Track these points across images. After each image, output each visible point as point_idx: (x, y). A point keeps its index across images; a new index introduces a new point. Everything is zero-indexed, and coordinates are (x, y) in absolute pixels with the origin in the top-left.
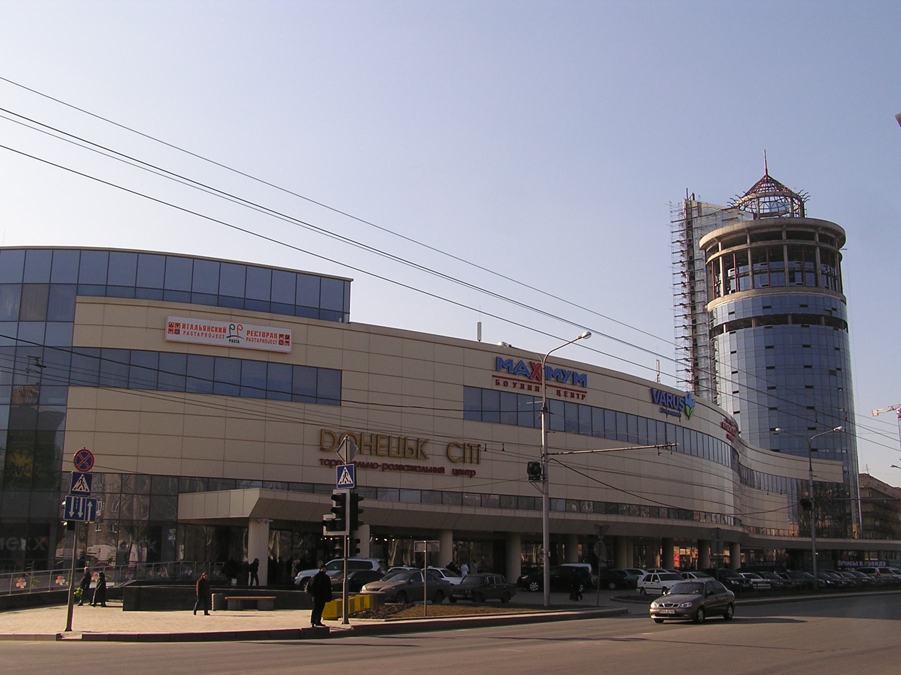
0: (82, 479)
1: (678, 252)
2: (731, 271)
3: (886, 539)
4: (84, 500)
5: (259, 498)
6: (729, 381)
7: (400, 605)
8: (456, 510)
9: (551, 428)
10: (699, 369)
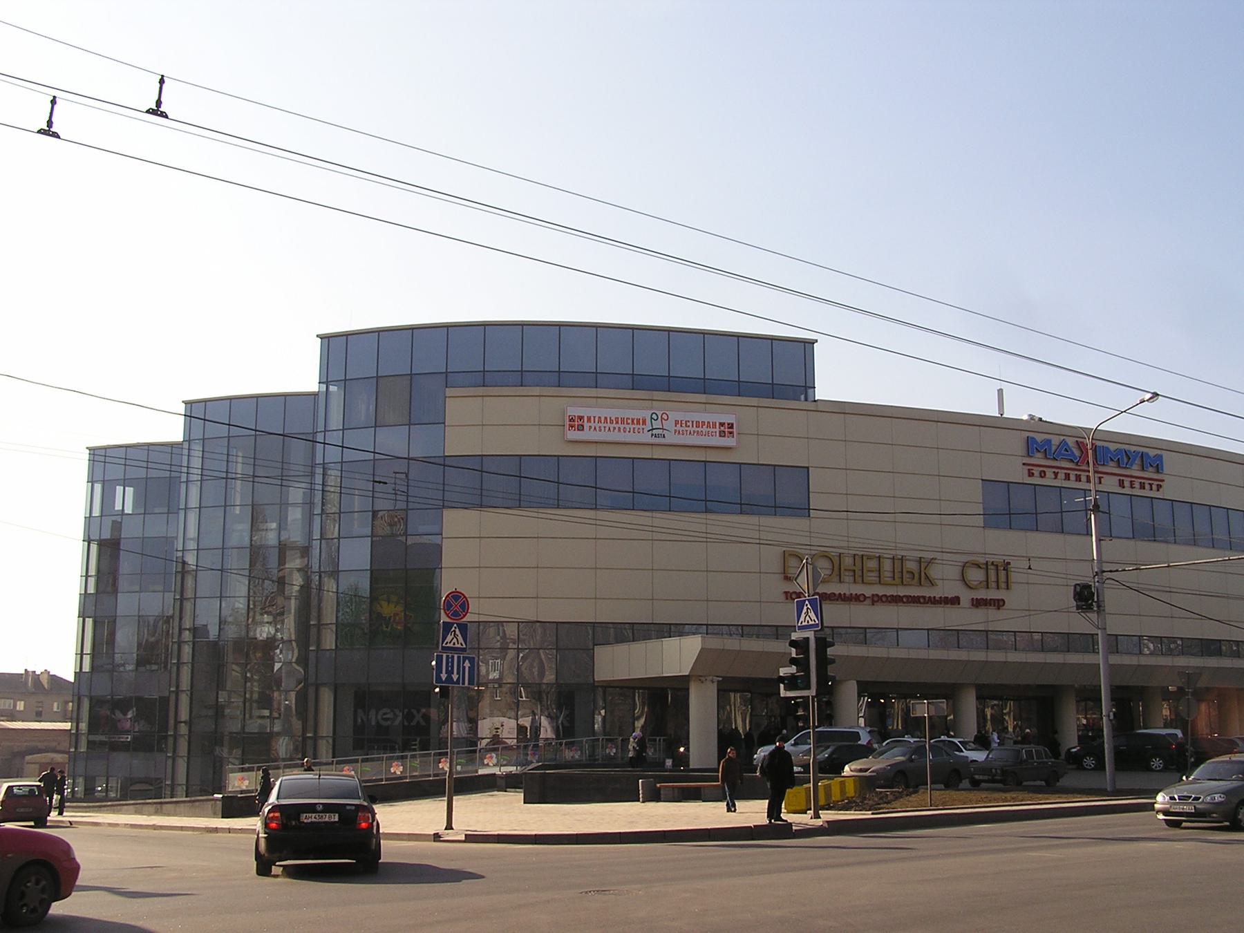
0: (454, 631)
4: (459, 658)
5: (702, 649)
7: (898, 792)
8: (979, 656)
9: (1113, 535)
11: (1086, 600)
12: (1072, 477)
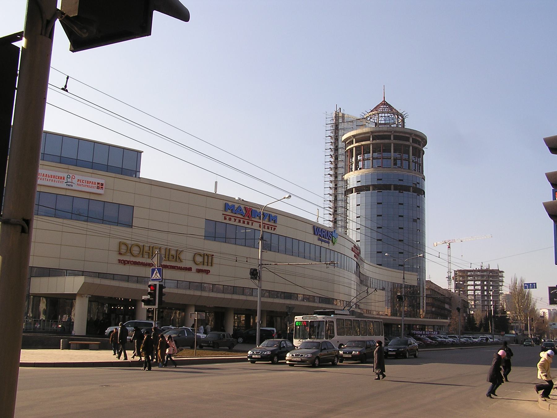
1: (329, 143)
2: (360, 156)
3: (438, 319)
5: (84, 282)
6: (359, 224)
8: (198, 293)
10: (337, 214)
11: (255, 275)
12: (242, 222)
